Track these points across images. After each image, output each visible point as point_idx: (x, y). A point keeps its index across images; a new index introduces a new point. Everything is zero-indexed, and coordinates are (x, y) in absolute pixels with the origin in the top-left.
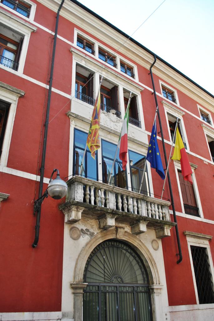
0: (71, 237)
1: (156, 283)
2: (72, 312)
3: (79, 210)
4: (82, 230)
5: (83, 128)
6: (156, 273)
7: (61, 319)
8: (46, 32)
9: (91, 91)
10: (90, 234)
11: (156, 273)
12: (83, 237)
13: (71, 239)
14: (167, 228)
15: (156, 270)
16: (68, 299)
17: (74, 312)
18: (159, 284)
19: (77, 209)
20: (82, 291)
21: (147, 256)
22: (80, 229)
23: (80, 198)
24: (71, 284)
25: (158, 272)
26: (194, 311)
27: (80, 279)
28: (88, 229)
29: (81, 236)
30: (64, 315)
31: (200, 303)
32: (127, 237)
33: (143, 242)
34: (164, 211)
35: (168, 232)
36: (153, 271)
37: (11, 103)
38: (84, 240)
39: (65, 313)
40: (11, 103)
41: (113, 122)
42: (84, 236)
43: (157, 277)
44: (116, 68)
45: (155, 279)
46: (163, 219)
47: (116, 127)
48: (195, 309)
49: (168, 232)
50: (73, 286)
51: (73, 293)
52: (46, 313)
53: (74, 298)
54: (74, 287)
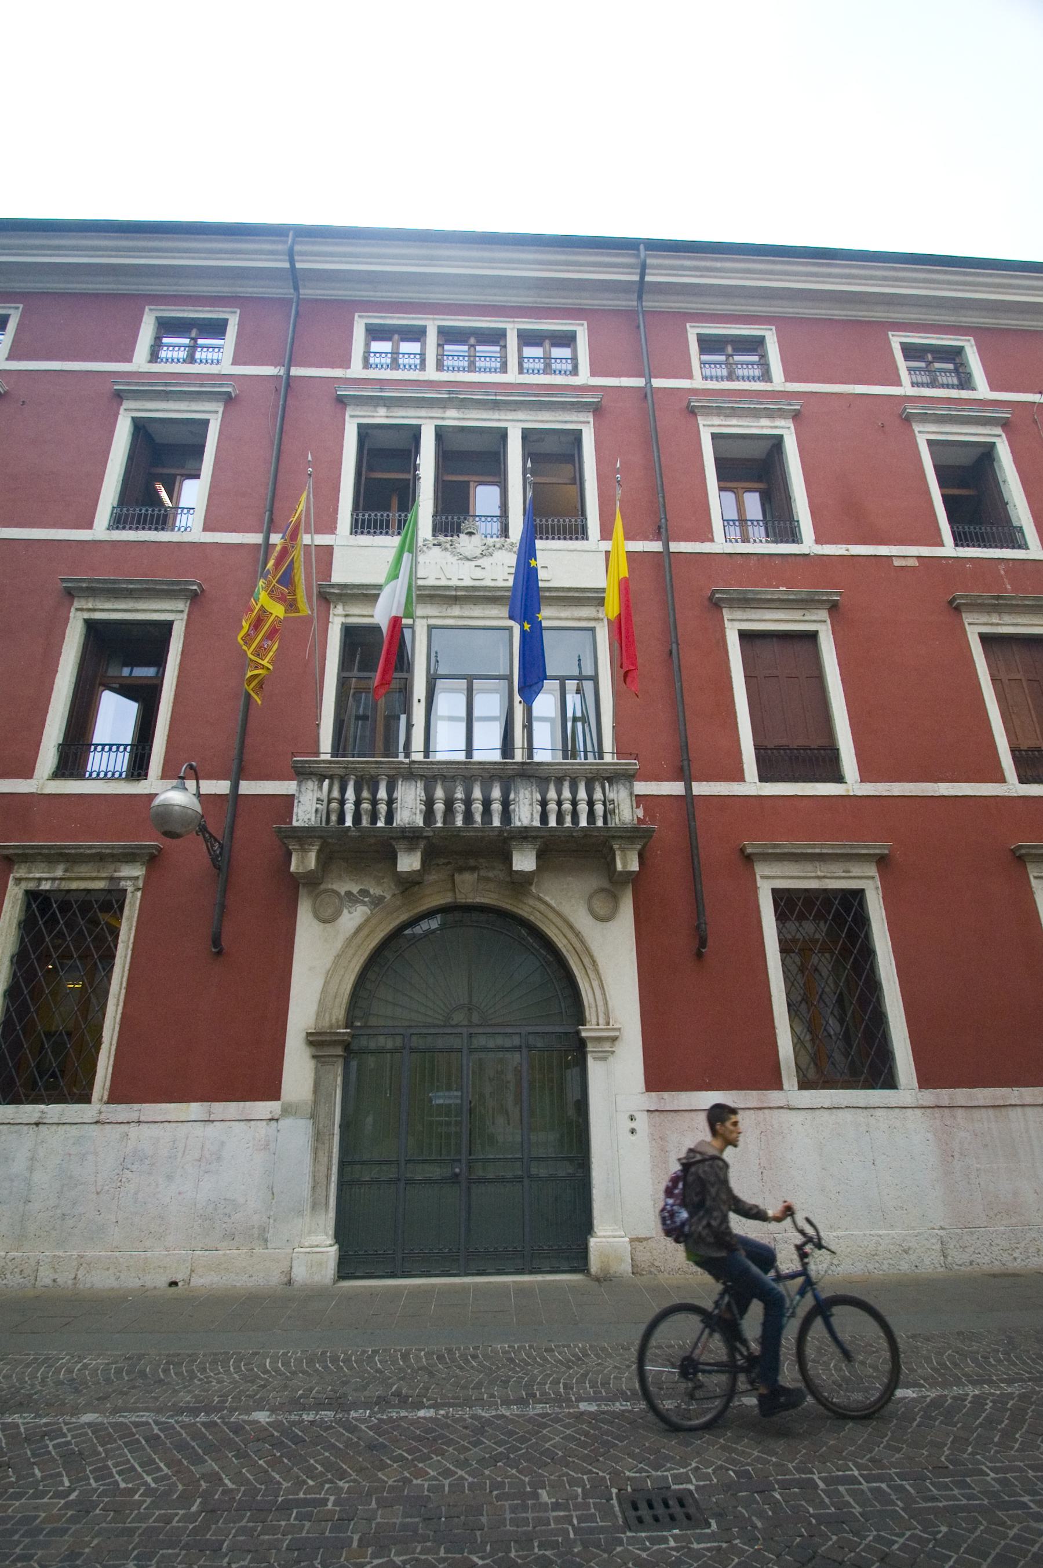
0: (317, 916)
1: (594, 1021)
2: (310, 1102)
3: (306, 847)
4: (349, 894)
5: (359, 616)
6: (598, 992)
7: (277, 1120)
8: (14, 341)
9: (361, 498)
10: (372, 903)
11: (598, 992)
12: (350, 912)
13: (316, 922)
14: (623, 850)
15: (595, 984)
16: (298, 1070)
17: (316, 1102)
18: (608, 1024)
19: (301, 845)
20: (339, 1051)
21: (565, 941)
22: (343, 893)
23: (308, 816)
24: (309, 1034)
25: (602, 987)
26: (766, 1111)
27: (334, 1021)
28: (367, 888)
29: (345, 911)
30: (286, 1111)
31: (805, 1084)
32: (492, 895)
33: (552, 903)
34: (611, 795)
35: (628, 862)
36: (587, 985)
37: (817, 632)
38: (352, 918)
39: (290, 1105)
40: (817, 632)
41: (468, 559)
42: (352, 910)
43: (600, 1003)
44: (1020, 547)
45: (593, 1010)
46: (605, 822)
47: (478, 573)
48: (771, 1105)
49: (628, 862)
50: (311, 1038)
51: (314, 1057)
52: (242, 1104)
53: (316, 1068)
54: (316, 1041)
